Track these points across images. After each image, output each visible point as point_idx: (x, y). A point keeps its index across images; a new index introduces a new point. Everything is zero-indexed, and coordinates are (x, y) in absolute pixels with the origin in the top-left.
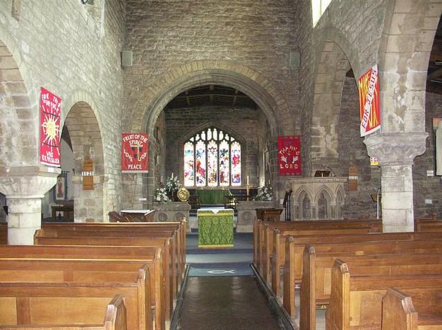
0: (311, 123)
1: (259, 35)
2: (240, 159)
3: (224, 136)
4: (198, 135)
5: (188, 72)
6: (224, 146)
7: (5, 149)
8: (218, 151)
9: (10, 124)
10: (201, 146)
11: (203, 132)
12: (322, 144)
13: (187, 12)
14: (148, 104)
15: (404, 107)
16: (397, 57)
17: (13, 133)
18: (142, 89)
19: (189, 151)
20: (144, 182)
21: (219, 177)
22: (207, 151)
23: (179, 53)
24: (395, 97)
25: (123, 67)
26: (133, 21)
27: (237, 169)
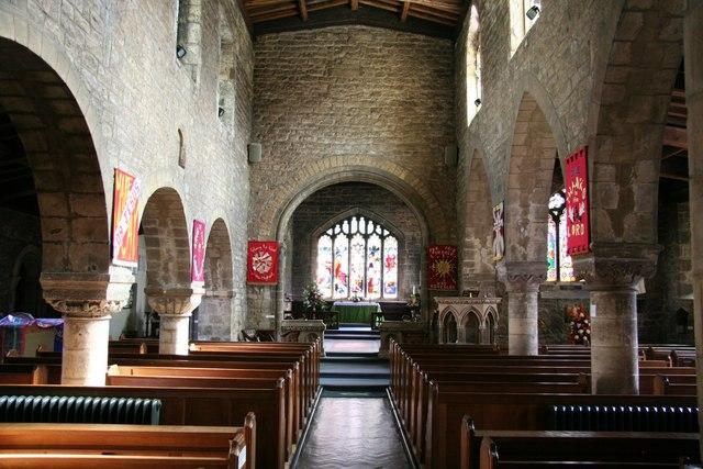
0: (464, 234)
1: (411, 124)
2: (396, 261)
3: (375, 227)
4: (338, 226)
5: (326, 169)
6: (374, 241)
7: (162, 273)
8: (366, 248)
9: (168, 251)
10: (341, 240)
11: (346, 222)
12: (477, 259)
13: (326, 95)
14: (278, 206)
15: (528, 238)
16: (519, 192)
17: (170, 259)
18: (272, 188)
19: (325, 249)
20: (272, 297)
21: (366, 285)
22: (350, 248)
23: (316, 146)
24: (518, 229)
25: (250, 162)
26: (262, 106)
27: (392, 275)
